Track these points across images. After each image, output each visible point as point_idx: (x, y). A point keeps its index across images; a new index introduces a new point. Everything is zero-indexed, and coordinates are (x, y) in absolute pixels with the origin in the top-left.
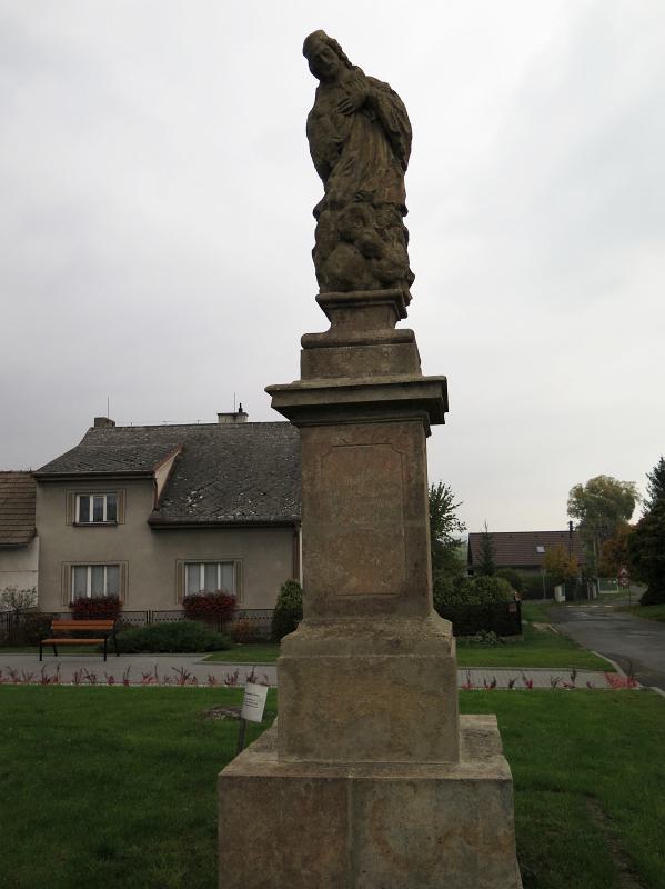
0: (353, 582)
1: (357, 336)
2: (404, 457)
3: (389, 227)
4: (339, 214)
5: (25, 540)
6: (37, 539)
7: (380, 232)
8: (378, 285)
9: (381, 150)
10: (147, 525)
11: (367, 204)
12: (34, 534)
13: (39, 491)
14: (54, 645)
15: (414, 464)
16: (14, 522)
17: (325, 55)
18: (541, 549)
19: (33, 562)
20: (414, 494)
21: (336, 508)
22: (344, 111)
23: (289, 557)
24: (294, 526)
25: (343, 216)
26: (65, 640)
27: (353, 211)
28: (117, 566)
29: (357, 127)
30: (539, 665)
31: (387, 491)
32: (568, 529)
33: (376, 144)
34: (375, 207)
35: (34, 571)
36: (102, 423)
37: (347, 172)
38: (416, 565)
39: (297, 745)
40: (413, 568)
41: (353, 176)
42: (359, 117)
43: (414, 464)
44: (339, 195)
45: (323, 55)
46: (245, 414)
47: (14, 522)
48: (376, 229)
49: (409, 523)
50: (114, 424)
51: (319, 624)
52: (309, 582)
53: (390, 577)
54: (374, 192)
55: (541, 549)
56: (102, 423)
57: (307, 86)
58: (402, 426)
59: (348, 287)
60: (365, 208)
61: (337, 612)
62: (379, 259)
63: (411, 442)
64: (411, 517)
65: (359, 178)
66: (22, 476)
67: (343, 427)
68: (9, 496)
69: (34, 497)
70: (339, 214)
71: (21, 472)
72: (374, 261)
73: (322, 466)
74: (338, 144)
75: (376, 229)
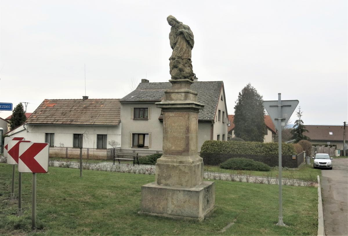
0: (173, 148)
1: (176, 91)
2: (185, 120)
3: (186, 64)
4: (174, 61)
5: (117, 124)
6: (121, 123)
7: (184, 65)
8: (183, 78)
9: (184, 45)
10: (158, 120)
11: (180, 59)
12: (120, 122)
13: (121, 107)
14: (119, 160)
15: (187, 122)
16: (113, 117)
17: (172, 22)
18: (331, 133)
19: (119, 132)
20: (187, 128)
21: (170, 131)
22: (176, 35)
23: (210, 134)
24: (211, 122)
25: (174, 62)
26: (129, 159)
27: (177, 61)
28: (148, 134)
29: (180, 39)
30: (212, 171)
31: (181, 127)
32: (344, 125)
33: (183, 44)
34: (182, 59)
35: (120, 135)
36: (145, 81)
37: (176, 50)
38: (187, 145)
39: (159, 183)
40: (186, 145)
41: (177, 52)
42: (180, 36)
43: (187, 122)
44: (174, 57)
45: (173, 22)
46: (197, 78)
47: (113, 117)
48: (183, 65)
49: (186, 135)
50: (148, 81)
51: (165, 157)
52: (164, 147)
53: (181, 147)
54: (182, 56)
55: (331, 133)
56: (145, 81)
57: (168, 28)
58: (185, 112)
59: (176, 78)
60: (180, 60)
61: (170, 154)
62: (183, 71)
63: (187, 116)
64: (186, 134)
65: (179, 52)
66: (117, 100)
67: (173, 112)
68: (112, 108)
69: (120, 109)
70: (174, 61)
71: (116, 99)
72: (182, 72)
73: (168, 121)
74: (175, 43)
75: (183, 65)
